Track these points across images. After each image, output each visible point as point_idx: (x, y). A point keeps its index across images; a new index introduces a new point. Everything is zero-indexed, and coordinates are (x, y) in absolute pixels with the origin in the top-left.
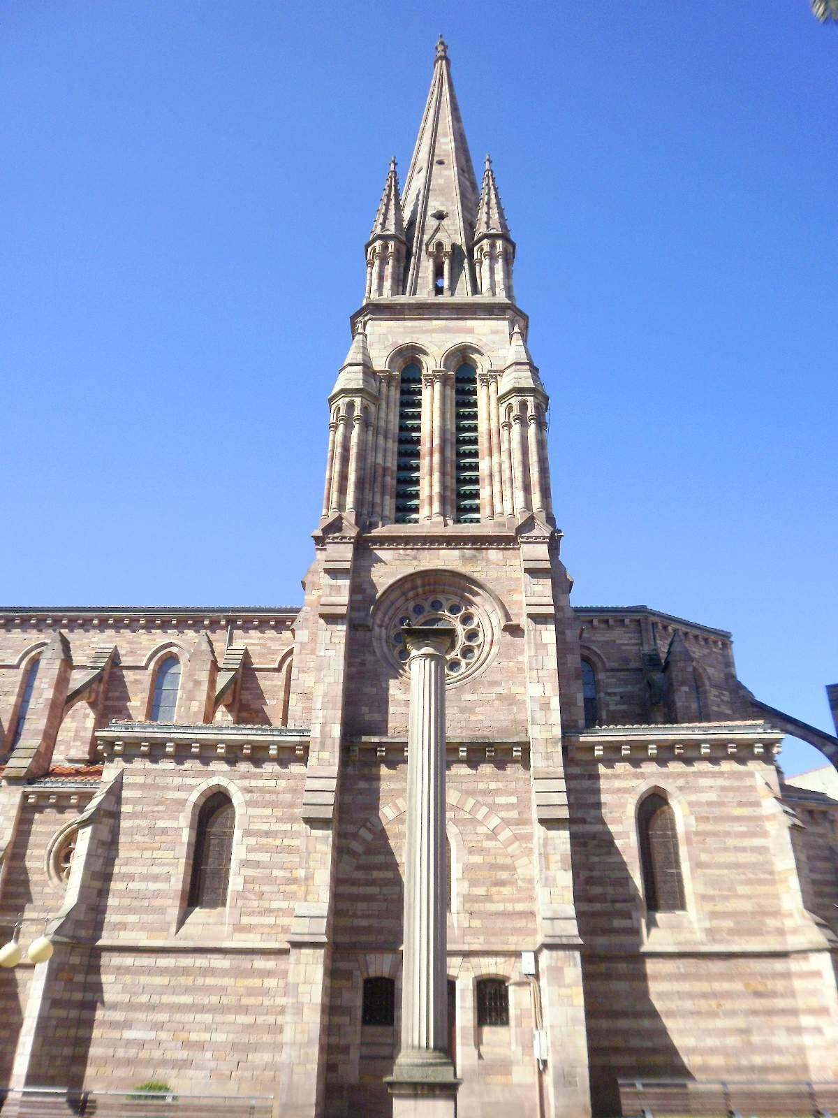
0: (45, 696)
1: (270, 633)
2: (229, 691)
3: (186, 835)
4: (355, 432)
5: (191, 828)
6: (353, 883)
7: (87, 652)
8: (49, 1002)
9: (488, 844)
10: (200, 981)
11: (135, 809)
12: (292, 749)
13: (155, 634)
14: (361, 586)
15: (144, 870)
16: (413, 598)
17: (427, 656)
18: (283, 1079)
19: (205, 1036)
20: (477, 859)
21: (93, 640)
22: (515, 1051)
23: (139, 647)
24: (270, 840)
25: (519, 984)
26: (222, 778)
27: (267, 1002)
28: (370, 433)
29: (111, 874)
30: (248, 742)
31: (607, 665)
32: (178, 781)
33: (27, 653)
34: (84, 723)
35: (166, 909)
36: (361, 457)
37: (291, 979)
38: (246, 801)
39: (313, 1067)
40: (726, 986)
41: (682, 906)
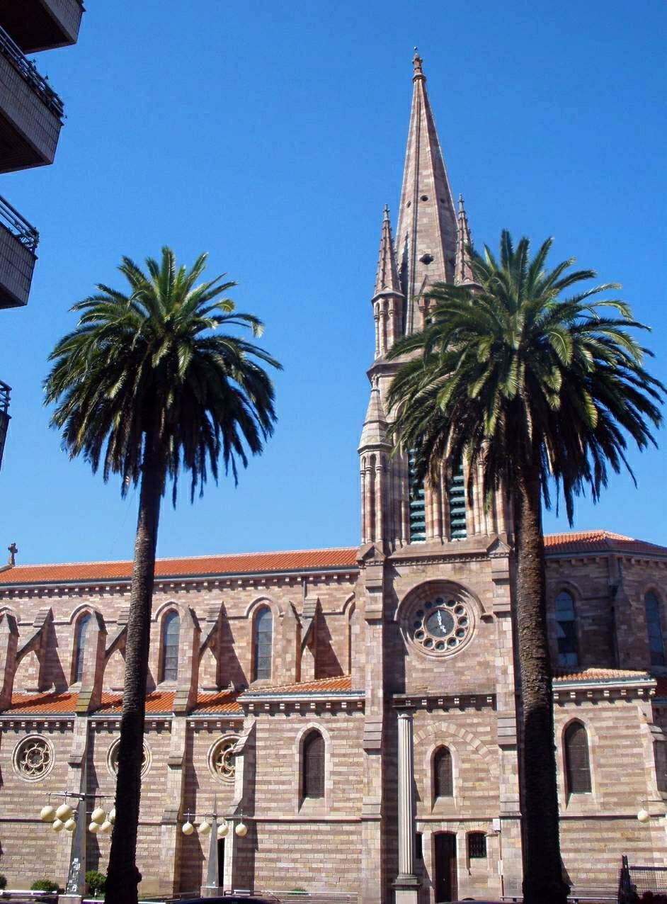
0: (187, 655)
1: (334, 585)
2: (311, 635)
3: (297, 758)
4: (378, 479)
7: (203, 607)
9: (473, 756)
10: (315, 837)
12: (355, 702)
16: (424, 598)
18: (364, 886)
19: (321, 865)
20: (467, 766)
21: (206, 597)
22: (490, 870)
23: (241, 601)
24: (346, 759)
25: (491, 836)
27: (352, 847)
28: (388, 476)
31: (582, 594)
32: (289, 726)
36: (384, 497)
37: (363, 837)
39: (379, 880)
40: (611, 835)
41: (589, 790)
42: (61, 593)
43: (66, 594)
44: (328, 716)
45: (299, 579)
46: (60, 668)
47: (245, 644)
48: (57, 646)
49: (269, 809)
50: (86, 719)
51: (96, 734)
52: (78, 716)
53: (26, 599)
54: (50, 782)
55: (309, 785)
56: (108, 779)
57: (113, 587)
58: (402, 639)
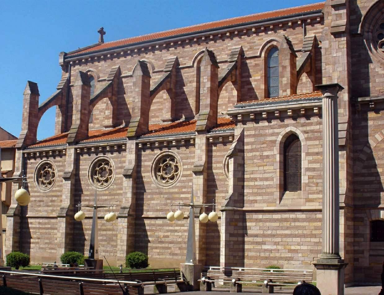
2: (307, 64)
5: (280, 154)
6: (363, 175)
7: (227, 52)
8: (228, 235)
10: (293, 224)
11: (252, 147)
13: (262, 36)
14: (355, 10)
15: (261, 176)
17: (327, 97)
19: (298, 247)
21: (229, 45)
23: (254, 45)
26: (292, 127)
29: (244, 178)
30: (303, 107)
32: (271, 131)
33: (196, 58)
34: (232, 93)
35: (273, 193)
38: (305, 138)
42: (126, 55)
43: (129, 55)
44: (303, 120)
45: (299, 22)
46: (127, 109)
47: (259, 78)
48: (125, 94)
49: (256, 201)
50: (135, 142)
51: (143, 153)
52: (129, 140)
53: (103, 63)
54: (113, 190)
55: (289, 180)
56: (153, 185)
57: (161, 45)
58: (366, 49)
